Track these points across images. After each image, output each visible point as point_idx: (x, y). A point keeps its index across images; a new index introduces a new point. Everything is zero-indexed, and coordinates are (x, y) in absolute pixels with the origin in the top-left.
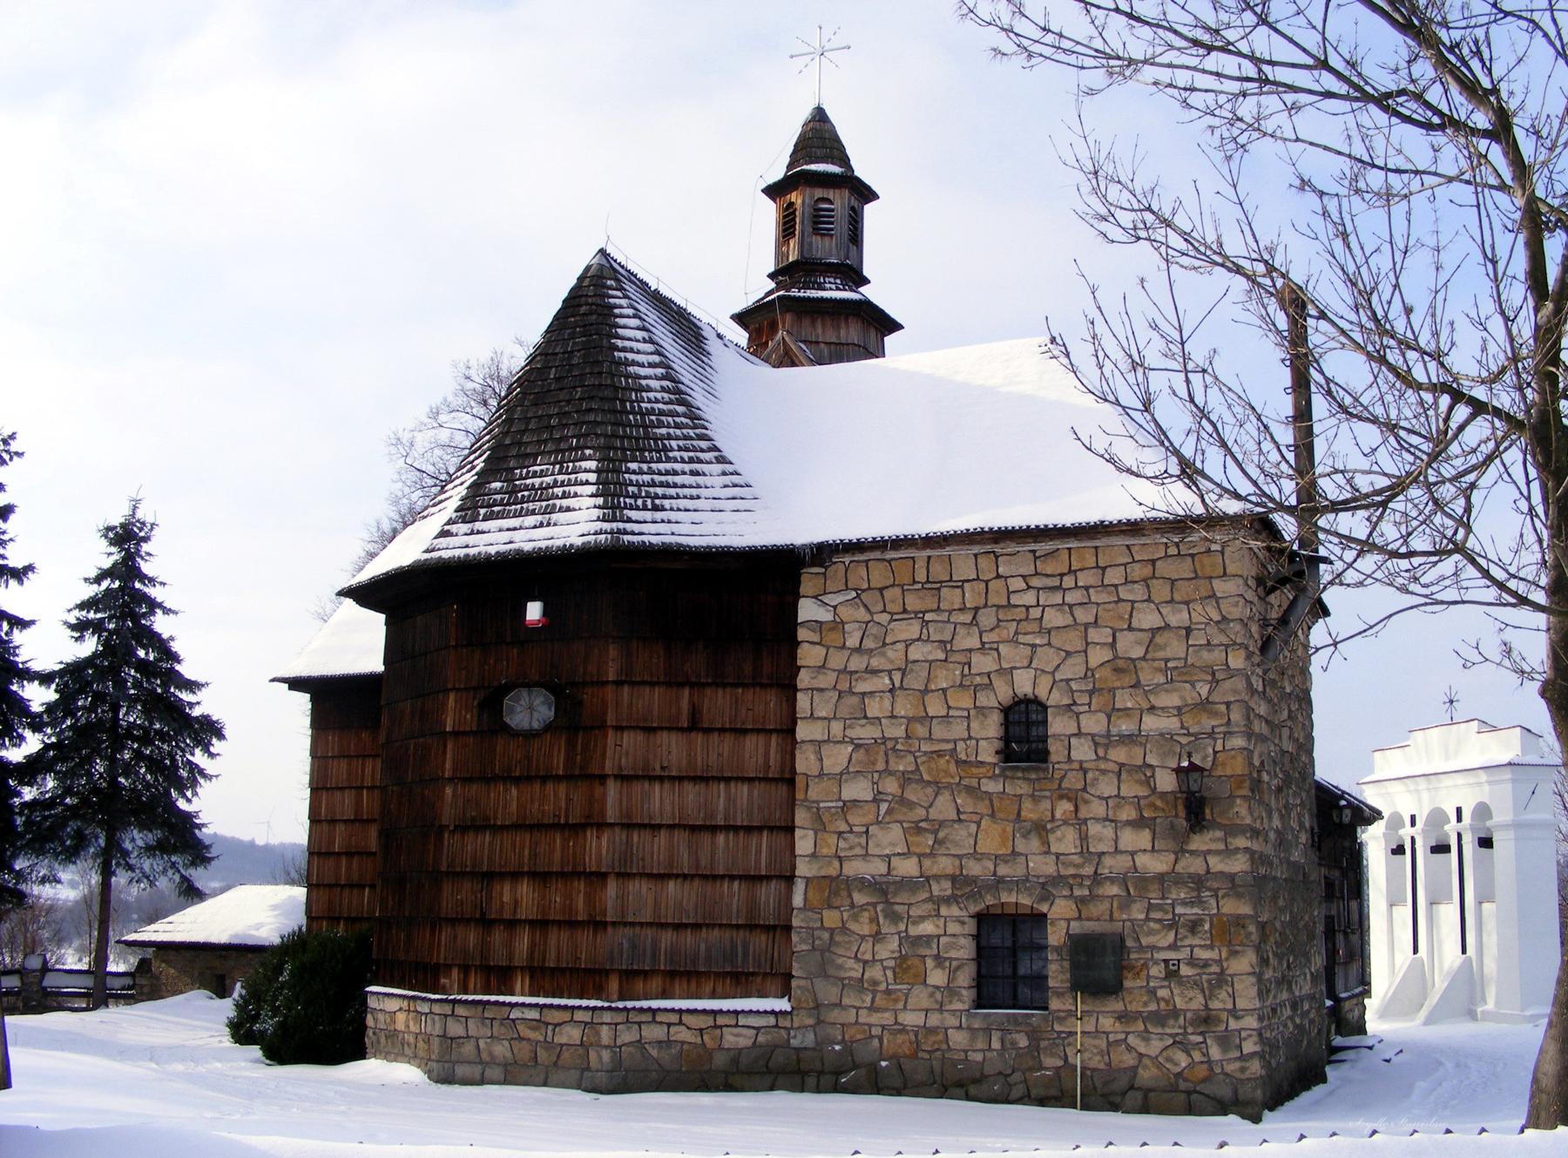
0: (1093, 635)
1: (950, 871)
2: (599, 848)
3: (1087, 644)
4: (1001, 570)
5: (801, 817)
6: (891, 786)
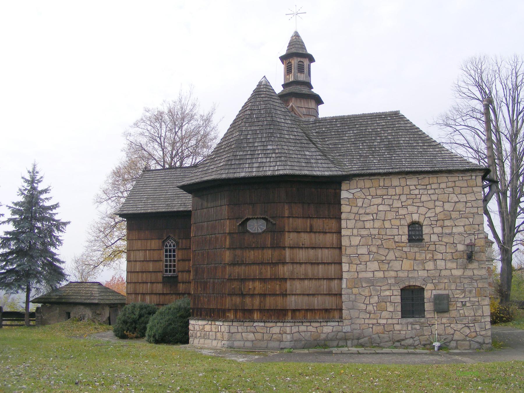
0: (437, 203)
2: (284, 270)
3: (435, 206)
4: (408, 183)
5: (344, 259)
6: (374, 249)
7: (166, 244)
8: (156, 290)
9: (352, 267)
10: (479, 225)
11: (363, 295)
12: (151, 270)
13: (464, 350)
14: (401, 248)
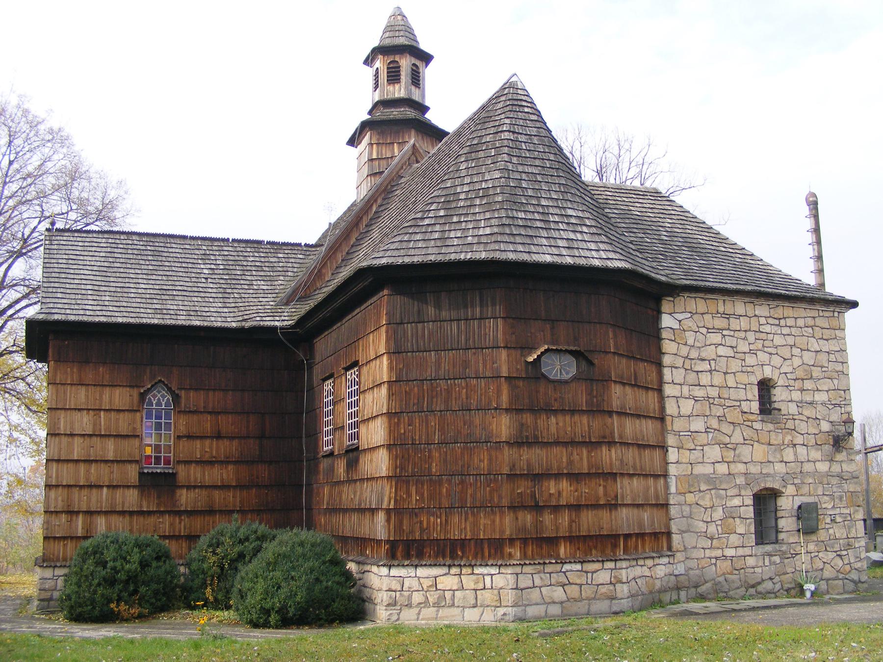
1: (743, 471)
3: (792, 355)
5: (671, 440)
6: (714, 423)
7: (150, 399)
8: (123, 503)
9: (683, 454)
10: (844, 391)
11: (701, 506)
12: (111, 456)
13: (837, 594)
14: (749, 424)
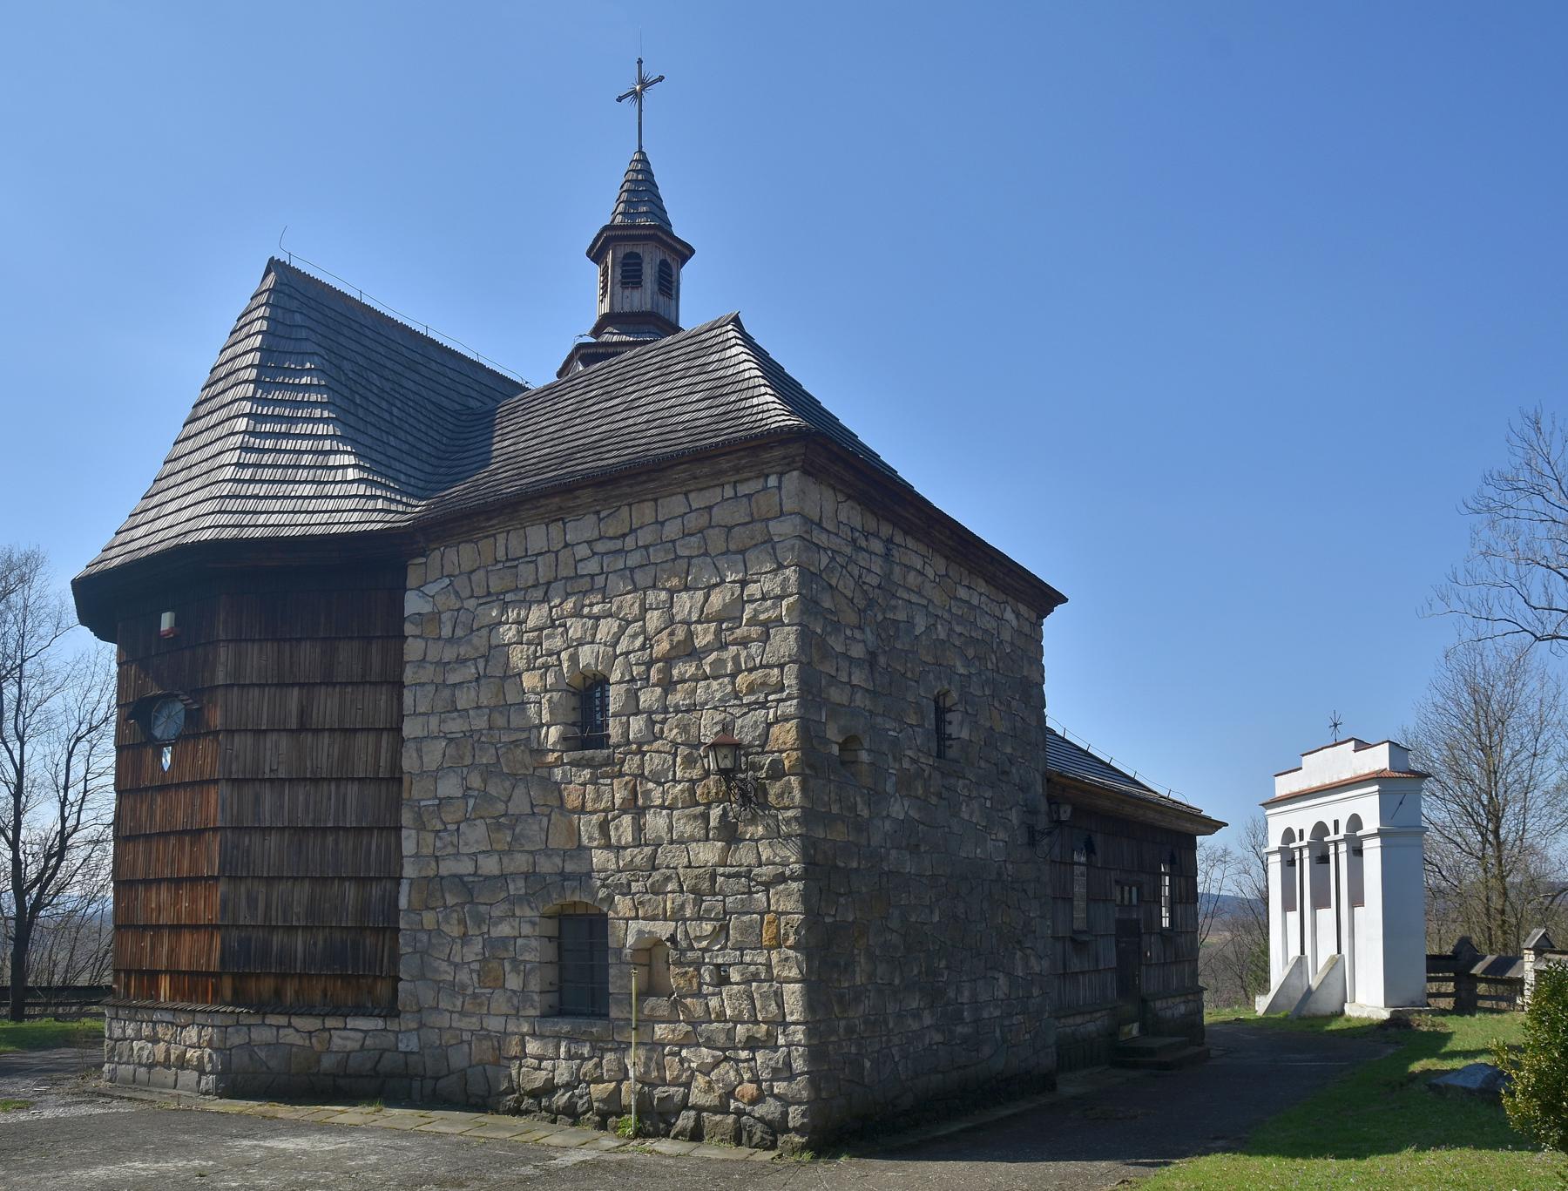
5: (407, 817)
